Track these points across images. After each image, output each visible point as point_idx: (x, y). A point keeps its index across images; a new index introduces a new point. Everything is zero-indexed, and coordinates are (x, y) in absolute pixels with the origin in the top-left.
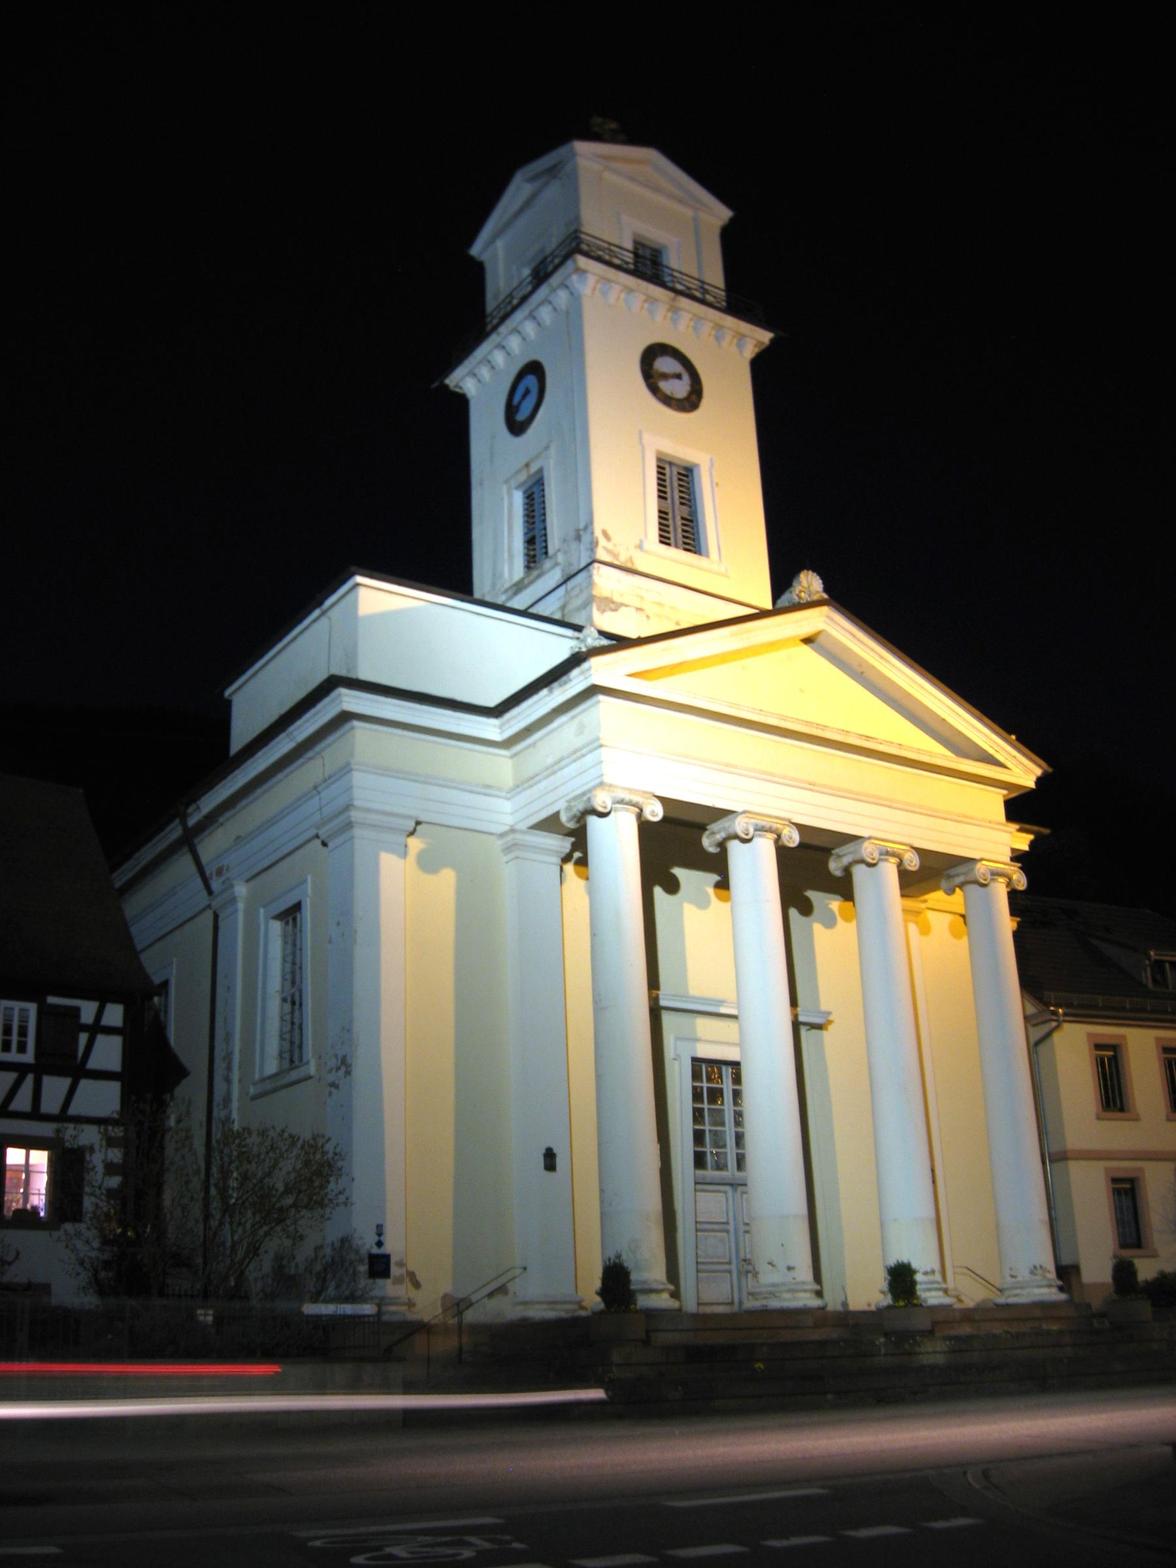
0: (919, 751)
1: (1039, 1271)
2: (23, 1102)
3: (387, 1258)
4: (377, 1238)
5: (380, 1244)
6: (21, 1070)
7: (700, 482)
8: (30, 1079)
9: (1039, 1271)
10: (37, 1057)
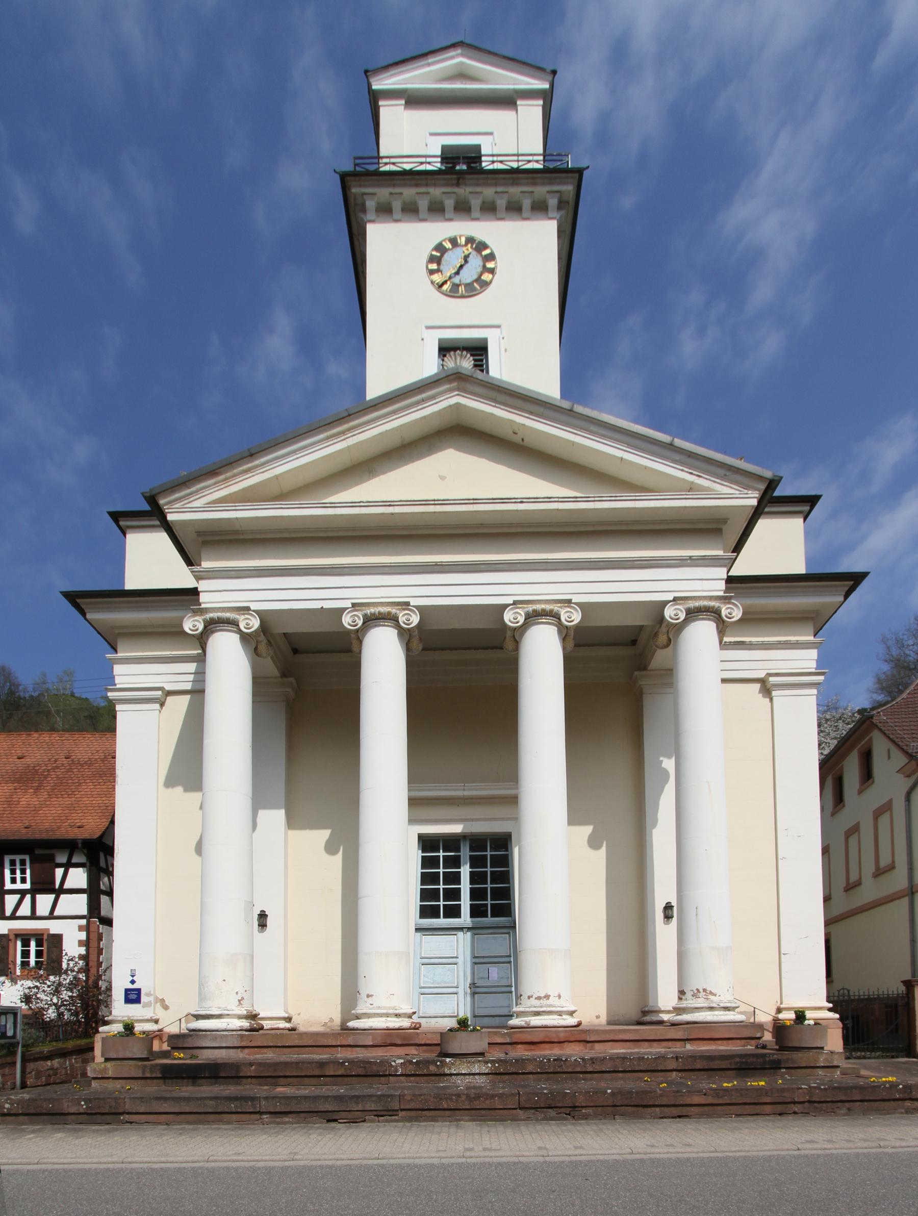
0: (536, 500)
1: (702, 994)
2: (25, 910)
3: (139, 991)
4: (131, 978)
5: (133, 982)
6: (23, 893)
7: (539, 394)
8: (28, 897)
9: (702, 994)
10: (32, 883)
